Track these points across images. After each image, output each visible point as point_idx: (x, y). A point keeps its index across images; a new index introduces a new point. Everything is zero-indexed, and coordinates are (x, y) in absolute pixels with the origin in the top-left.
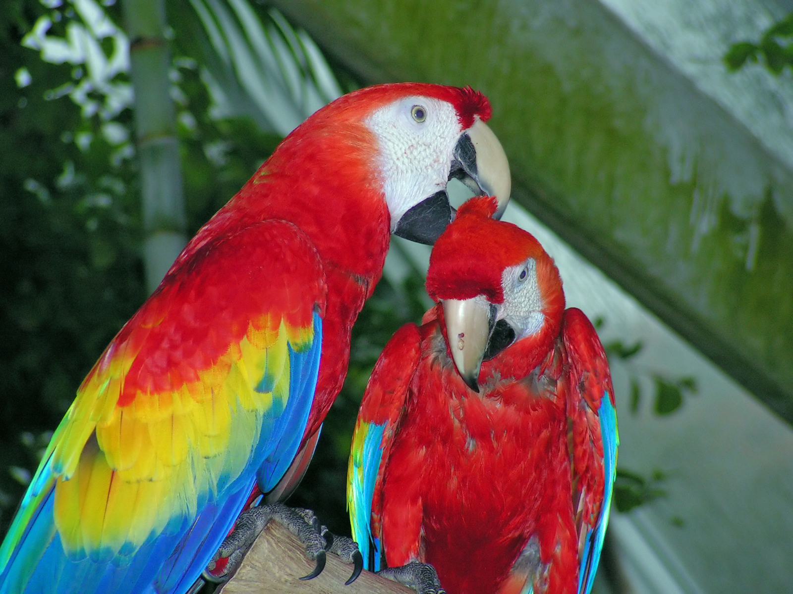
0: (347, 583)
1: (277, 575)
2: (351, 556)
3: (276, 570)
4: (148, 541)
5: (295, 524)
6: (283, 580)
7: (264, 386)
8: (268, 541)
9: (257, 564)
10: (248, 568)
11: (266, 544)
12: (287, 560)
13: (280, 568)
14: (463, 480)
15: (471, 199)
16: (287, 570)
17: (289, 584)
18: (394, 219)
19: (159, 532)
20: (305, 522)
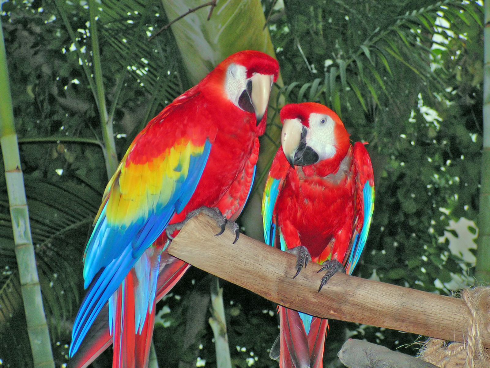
0: (233, 244)
1: (198, 236)
2: (235, 231)
3: (197, 234)
4: (131, 225)
5: (211, 213)
6: (200, 238)
7: (178, 169)
8: (194, 222)
9: (188, 231)
10: (184, 232)
11: (193, 223)
12: (203, 230)
13: (199, 233)
14: (303, 214)
15: (292, 225)
16: (203, 234)
17: (203, 240)
18: (346, 164)
19: (134, 222)
20: (215, 212)
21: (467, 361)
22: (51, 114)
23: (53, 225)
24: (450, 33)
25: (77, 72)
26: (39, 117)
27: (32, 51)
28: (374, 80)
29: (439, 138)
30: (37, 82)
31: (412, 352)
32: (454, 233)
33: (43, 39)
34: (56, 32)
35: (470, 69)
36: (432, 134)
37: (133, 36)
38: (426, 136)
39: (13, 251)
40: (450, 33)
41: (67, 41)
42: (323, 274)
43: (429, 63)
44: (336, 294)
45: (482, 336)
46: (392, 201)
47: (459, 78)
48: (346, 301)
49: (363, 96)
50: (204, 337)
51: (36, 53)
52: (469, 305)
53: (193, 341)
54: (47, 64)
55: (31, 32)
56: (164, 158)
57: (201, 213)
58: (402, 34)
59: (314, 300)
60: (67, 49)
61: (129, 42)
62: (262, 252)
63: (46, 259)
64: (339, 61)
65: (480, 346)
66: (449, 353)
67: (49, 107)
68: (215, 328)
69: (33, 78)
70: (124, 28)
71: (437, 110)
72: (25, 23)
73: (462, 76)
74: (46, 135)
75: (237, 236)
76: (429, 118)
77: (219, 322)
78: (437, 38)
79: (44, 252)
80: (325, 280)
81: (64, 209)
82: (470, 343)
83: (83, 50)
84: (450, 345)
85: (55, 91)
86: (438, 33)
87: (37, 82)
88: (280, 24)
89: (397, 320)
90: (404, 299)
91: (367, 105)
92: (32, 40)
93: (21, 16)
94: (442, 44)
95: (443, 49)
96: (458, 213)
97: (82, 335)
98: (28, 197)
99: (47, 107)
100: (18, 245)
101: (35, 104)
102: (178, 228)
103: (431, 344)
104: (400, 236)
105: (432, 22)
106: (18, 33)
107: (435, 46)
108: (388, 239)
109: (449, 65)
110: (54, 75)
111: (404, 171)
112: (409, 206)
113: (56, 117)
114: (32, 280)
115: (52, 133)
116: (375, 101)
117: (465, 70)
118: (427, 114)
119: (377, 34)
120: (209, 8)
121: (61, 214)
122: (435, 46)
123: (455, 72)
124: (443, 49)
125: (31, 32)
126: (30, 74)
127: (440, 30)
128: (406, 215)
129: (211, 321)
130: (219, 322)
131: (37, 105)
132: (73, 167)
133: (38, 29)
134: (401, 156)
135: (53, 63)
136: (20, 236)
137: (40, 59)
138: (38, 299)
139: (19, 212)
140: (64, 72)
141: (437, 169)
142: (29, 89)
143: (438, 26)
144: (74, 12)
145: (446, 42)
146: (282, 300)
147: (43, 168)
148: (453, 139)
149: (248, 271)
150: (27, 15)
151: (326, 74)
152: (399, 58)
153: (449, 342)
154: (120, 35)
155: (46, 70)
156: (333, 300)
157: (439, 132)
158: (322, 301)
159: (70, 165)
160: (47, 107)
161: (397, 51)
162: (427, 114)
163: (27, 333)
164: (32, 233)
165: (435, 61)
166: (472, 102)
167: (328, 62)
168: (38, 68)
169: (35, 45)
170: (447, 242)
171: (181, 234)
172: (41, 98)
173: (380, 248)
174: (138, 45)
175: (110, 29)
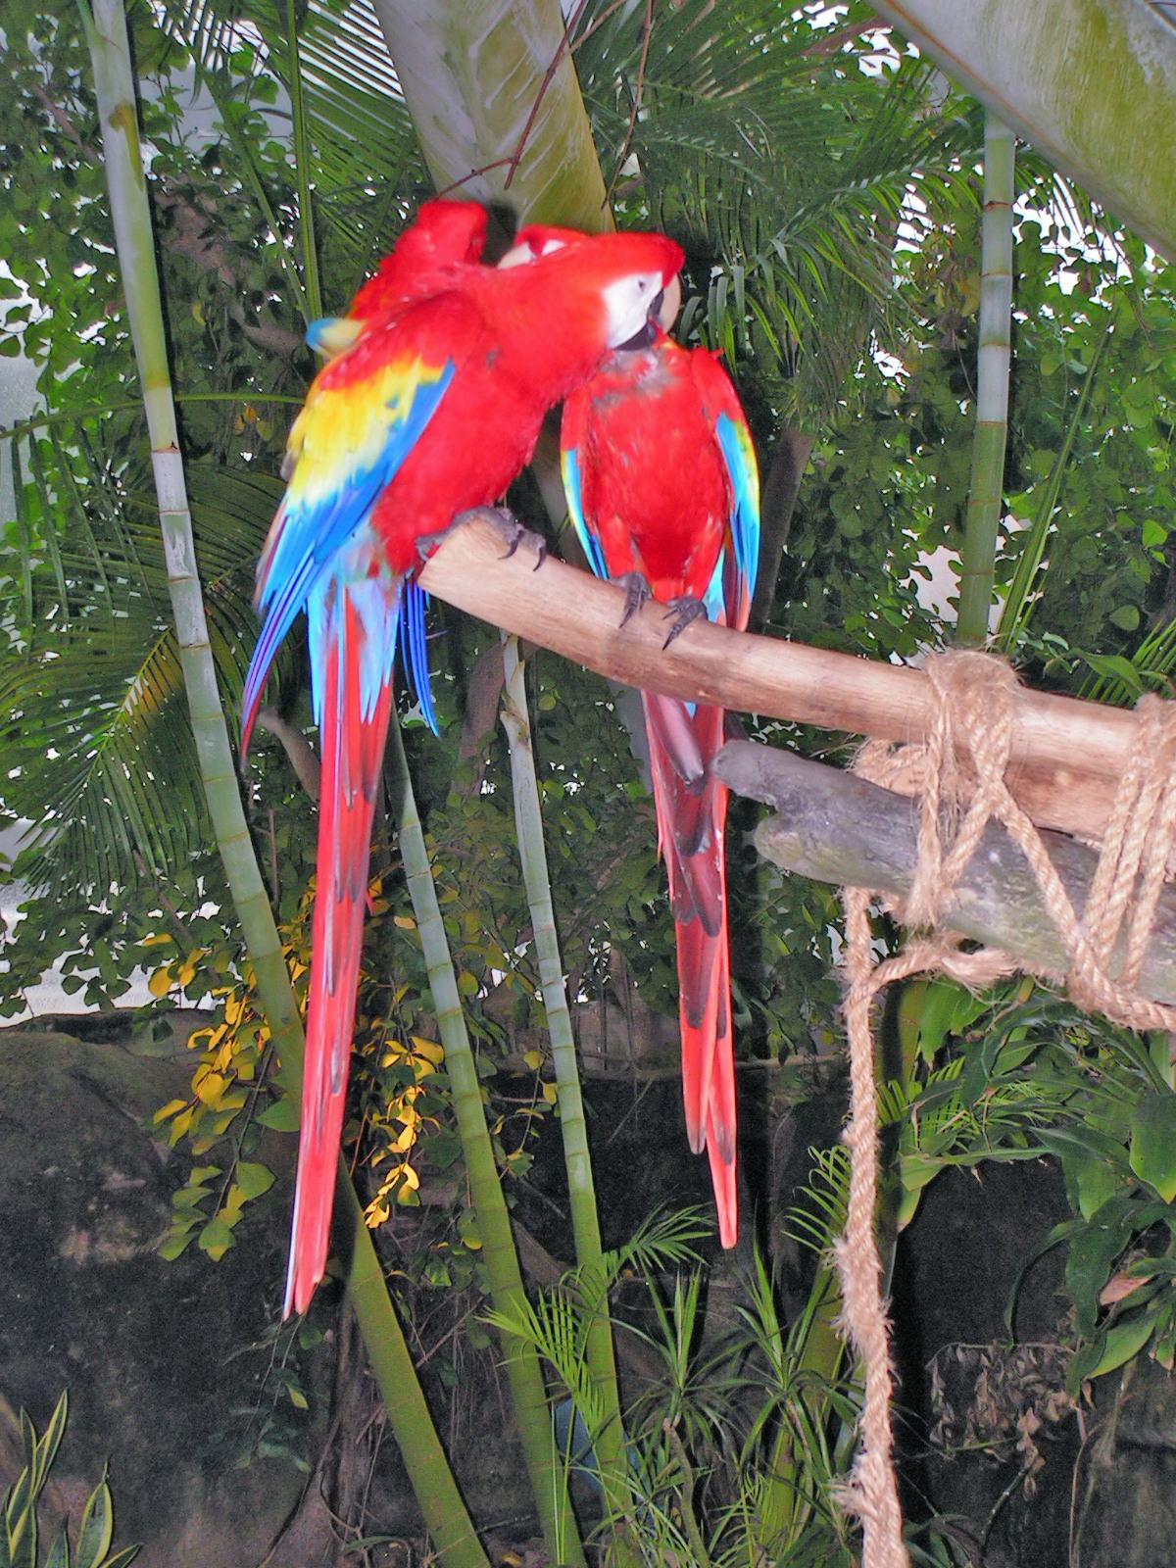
21: (926, 777)
22: (235, 354)
23: (234, 547)
24: (925, 222)
25: (277, 282)
26: (212, 360)
27: (202, 243)
28: (790, 301)
29: (903, 408)
30: (210, 298)
31: (836, 762)
32: (926, 573)
33: (220, 221)
34: (242, 209)
35: (959, 287)
36: (893, 399)
37: (374, 216)
38: (881, 401)
39: (166, 589)
40: (925, 222)
41: (261, 226)
42: (675, 618)
43: (889, 276)
44: (710, 662)
45: (954, 733)
46: (821, 516)
47: (939, 301)
48: (726, 675)
49: (775, 331)
50: (494, 743)
51: (208, 247)
52: (936, 681)
53: (476, 751)
54: (549, 558)
55: (200, 210)
56: (373, 384)
57: (477, 518)
58: (842, 219)
59: (671, 672)
60: (262, 241)
61: (368, 227)
62: (582, 589)
63: (222, 606)
64: (734, 268)
65: (950, 750)
66: (897, 762)
67: (230, 344)
68: (512, 729)
69: (203, 291)
70: (359, 203)
71: (902, 358)
72: (189, 194)
73: (944, 298)
74: (224, 389)
75: (542, 558)
76: (888, 372)
77: (519, 720)
78: (905, 230)
79: (220, 594)
80: (676, 630)
81: (252, 520)
82: (933, 745)
83: (288, 242)
84: (901, 750)
85: (240, 314)
86: (905, 221)
87: (210, 298)
88: (633, 201)
89: (813, 707)
90: (826, 672)
91: (781, 348)
92: (202, 223)
93: (182, 183)
94: (912, 241)
95: (915, 250)
96: (934, 538)
97: (727, 1210)
98: (190, 498)
99: (227, 343)
100: (174, 579)
101: (206, 338)
102: (438, 541)
103: (870, 747)
104: (833, 577)
105: (896, 200)
106: (177, 212)
107: (901, 246)
108: (813, 583)
109: (922, 279)
110: (239, 286)
111: (844, 465)
112: (850, 525)
113: (240, 362)
114: (198, 640)
115: (235, 389)
116: (795, 338)
117: (951, 287)
118: (885, 365)
119: (799, 220)
120: (507, 168)
121: (247, 527)
122: (901, 246)
123: (933, 291)
124: (915, 250)
125: (200, 210)
126: (197, 286)
127: (909, 216)
128: (846, 542)
129: (503, 716)
130: (519, 720)
131: (210, 342)
132: (271, 449)
133: (211, 205)
134: (838, 438)
135: (237, 266)
136: (178, 563)
137: (215, 258)
138: (209, 672)
139: (175, 521)
140: (255, 282)
141: (901, 461)
142: (196, 310)
143: (905, 208)
144: (274, 175)
145: (920, 238)
146: (616, 672)
147: (219, 450)
148: (928, 408)
149: (557, 621)
150: (194, 181)
151: (711, 289)
152: (837, 264)
153: (898, 745)
154: (352, 215)
155: (225, 277)
156: (703, 672)
157: (904, 396)
158: (685, 674)
159: (265, 444)
160: (227, 343)
161: (834, 251)
162: (885, 365)
163: (189, 727)
164: (198, 560)
165: (900, 271)
166: (963, 344)
167: (717, 270)
168: (212, 272)
169: (207, 233)
170: (913, 586)
171: (442, 553)
172: (217, 326)
173: (800, 597)
174: (381, 234)
175: (333, 204)
